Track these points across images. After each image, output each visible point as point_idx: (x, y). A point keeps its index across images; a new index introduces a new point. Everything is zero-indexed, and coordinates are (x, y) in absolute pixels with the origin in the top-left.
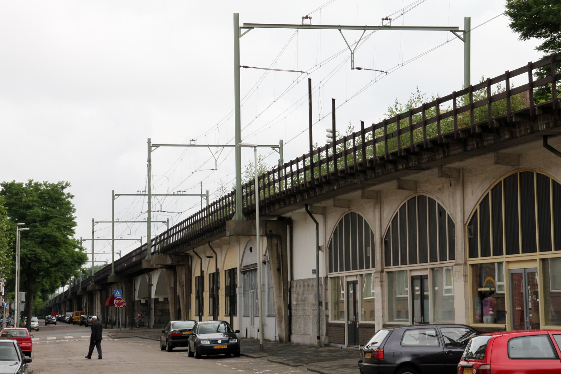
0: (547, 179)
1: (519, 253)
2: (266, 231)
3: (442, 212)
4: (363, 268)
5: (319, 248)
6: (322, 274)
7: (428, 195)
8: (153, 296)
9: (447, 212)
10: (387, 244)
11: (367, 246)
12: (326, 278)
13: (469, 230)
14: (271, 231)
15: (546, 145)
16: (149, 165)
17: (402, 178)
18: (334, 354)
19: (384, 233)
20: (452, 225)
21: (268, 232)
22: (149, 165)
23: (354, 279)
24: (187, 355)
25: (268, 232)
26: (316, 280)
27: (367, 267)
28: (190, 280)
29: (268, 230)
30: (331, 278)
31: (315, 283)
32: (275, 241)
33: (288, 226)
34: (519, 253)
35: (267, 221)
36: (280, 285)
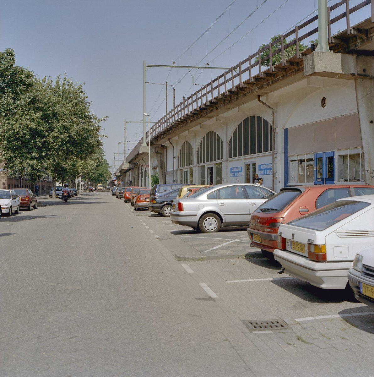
0: (261, 118)
1: (248, 154)
2: (156, 151)
3: (219, 138)
4: (220, 160)
5: (174, 157)
6: (175, 169)
7: (214, 131)
8: (130, 180)
9: (221, 138)
10: (198, 154)
11: (191, 155)
12: (177, 170)
13: (229, 145)
14: (158, 151)
15: (259, 100)
16: (174, 96)
17: (203, 123)
18: (363, 177)
19: (197, 150)
20: (222, 142)
21: (157, 152)
22: (174, 96)
23: (186, 170)
24: (312, 184)
25: (157, 152)
26: (173, 171)
27: (219, 159)
28: (139, 173)
29: (157, 150)
30: (179, 170)
31: (173, 172)
32: (159, 155)
33: (165, 149)
34: (255, 153)
35: (156, 147)
36: (161, 173)
